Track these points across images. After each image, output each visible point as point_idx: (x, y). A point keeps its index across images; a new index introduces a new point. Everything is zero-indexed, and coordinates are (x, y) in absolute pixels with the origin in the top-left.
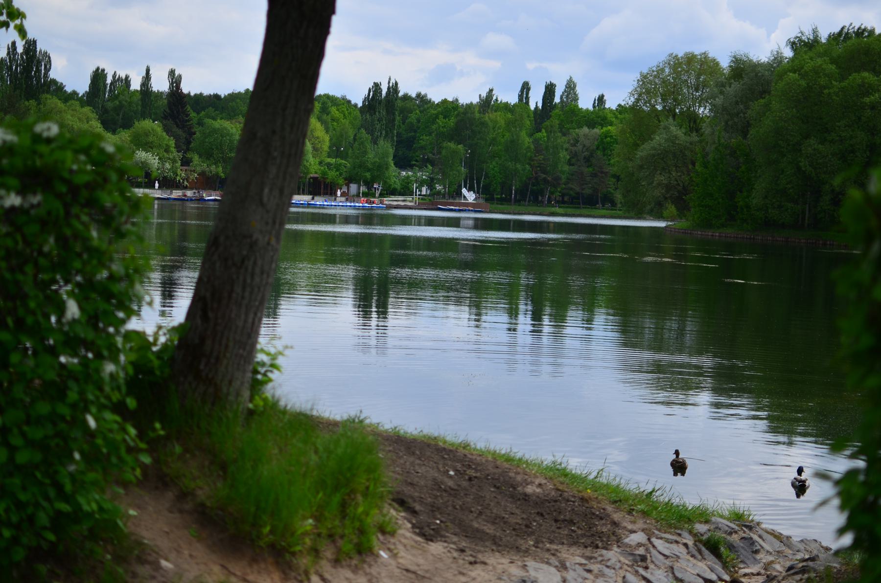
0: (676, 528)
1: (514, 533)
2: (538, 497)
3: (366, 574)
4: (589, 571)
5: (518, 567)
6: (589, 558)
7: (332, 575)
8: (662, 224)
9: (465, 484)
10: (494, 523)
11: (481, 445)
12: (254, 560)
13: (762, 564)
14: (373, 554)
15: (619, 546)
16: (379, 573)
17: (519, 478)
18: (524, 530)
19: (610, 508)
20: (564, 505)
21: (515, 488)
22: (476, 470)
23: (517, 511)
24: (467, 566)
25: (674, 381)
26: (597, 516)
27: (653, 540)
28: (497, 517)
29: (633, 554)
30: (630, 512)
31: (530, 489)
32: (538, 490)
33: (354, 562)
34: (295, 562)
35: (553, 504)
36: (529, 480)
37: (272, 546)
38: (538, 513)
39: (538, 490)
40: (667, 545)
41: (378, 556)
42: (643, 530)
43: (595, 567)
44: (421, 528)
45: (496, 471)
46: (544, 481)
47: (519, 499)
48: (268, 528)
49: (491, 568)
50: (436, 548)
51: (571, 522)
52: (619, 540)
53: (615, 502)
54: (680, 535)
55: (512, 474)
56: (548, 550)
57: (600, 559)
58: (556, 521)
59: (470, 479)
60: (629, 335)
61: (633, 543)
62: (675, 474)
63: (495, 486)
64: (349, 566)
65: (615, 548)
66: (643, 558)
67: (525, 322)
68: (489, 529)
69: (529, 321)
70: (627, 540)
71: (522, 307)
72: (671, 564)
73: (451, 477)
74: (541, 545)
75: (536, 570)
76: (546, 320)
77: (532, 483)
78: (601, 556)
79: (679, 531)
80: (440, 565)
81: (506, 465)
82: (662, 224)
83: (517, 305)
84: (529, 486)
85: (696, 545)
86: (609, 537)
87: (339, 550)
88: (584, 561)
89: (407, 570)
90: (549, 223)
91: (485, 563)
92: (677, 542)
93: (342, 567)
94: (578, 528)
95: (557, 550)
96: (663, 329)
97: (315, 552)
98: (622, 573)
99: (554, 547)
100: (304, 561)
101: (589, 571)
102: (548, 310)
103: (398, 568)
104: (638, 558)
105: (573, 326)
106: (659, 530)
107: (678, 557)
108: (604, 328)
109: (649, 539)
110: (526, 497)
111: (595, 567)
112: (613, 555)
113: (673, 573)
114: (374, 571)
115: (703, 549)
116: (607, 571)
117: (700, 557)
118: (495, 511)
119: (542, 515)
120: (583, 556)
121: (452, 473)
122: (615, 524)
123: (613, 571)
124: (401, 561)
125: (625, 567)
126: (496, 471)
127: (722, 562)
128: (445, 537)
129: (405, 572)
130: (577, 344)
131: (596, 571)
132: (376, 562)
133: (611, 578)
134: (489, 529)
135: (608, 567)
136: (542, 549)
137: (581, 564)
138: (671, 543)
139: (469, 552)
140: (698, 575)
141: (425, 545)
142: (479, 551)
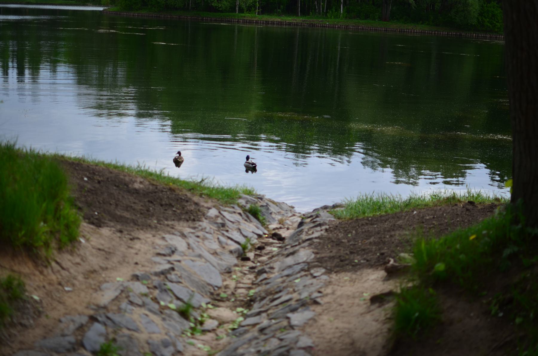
0: (230, 203)
1: (142, 216)
2: (144, 190)
3: (79, 255)
4: (198, 237)
5: (159, 239)
6: (194, 228)
7: (60, 259)
8: (101, 9)
9: (97, 186)
10: (127, 211)
11: (73, 156)
12: (14, 256)
13: (277, 222)
14: (77, 241)
15: (206, 219)
16: (85, 254)
17: (127, 179)
18: (147, 214)
19: (189, 194)
20: (161, 195)
21: (127, 186)
22: (100, 176)
23: (137, 201)
24: (130, 241)
25: (108, 108)
26: (184, 200)
27: (222, 212)
28: (127, 206)
29: (217, 223)
30: (201, 195)
31: (137, 186)
32: (141, 186)
33: (69, 248)
34: (40, 253)
35: (154, 194)
36: (133, 179)
37: (25, 245)
38: (149, 201)
39: (141, 186)
40: (231, 215)
41: (80, 242)
42: (214, 207)
43: (200, 234)
44: (89, 219)
45: (111, 175)
46: (142, 180)
47: (134, 193)
48: (23, 232)
49: (144, 241)
50: (105, 231)
51: (171, 206)
52: (204, 215)
53: (190, 190)
54: (233, 208)
55: (122, 177)
56: (168, 225)
57: (200, 228)
58: (162, 205)
59: (99, 182)
60: (82, 79)
61: (213, 216)
62: (247, 171)
63: (115, 186)
64: (67, 251)
65: (205, 220)
66: (223, 225)
67: (13, 73)
68: (127, 215)
69: (15, 71)
70: (209, 214)
71: (10, 64)
72: (237, 227)
73: (86, 182)
74: (162, 222)
75: (171, 239)
76: (27, 72)
77: (136, 181)
78: (200, 226)
79: (232, 205)
80: (114, 243)
81: (116, 171)
82: (101, 9)
83: (8, 62)
84: (135, 184)
85: (245, 214)
86: (197, 213)
87: (59, 241)
88: (193, 231)
89: (99, 249)
90: (25, 9)
91: (138, 239)
92: (235, 212)
93: (63, 252)
94: (177, 208)
95: (172, 225)
96: (103, 74)
97: (47, 245)
98: (216, 236)
99: (170, 223)
100: (43, 252)
101: (198, 237)
102: (27, 66)
103: (93, 248)
104: (220, 225)
105: (44, 73)
106: (222, 206)
107: (239, 222)
108: (65, 74)
109: (220, 212)
110: (137, 191)
111: (200, 234)
112: (205, 223)
113: (241, 233)
114: (82, 252)
115: (250, 215)
116: (208, 235)
117: (248, 220)
118: (124, 202)
119: (152, 202)
120: (189, 227)
121: (86, 179)
122: (196, 204)
123: (211, 235)
124: (92, 243)
125: (216, 232)
126: (111, 175)
127: (260, 222)
128: (106, 223)
129: (98, 251)
130: (47, 87)
131: (202, 236)
132: (80, 246)
133: (211, 239)
134: (127, 215)
135: (207, 233)
136: (164, 225)
137: (192, 233)
138: (232, 213)
139: (126, 232)
140: (253, 232)
141: (97, 230)
142: (131, 231)
